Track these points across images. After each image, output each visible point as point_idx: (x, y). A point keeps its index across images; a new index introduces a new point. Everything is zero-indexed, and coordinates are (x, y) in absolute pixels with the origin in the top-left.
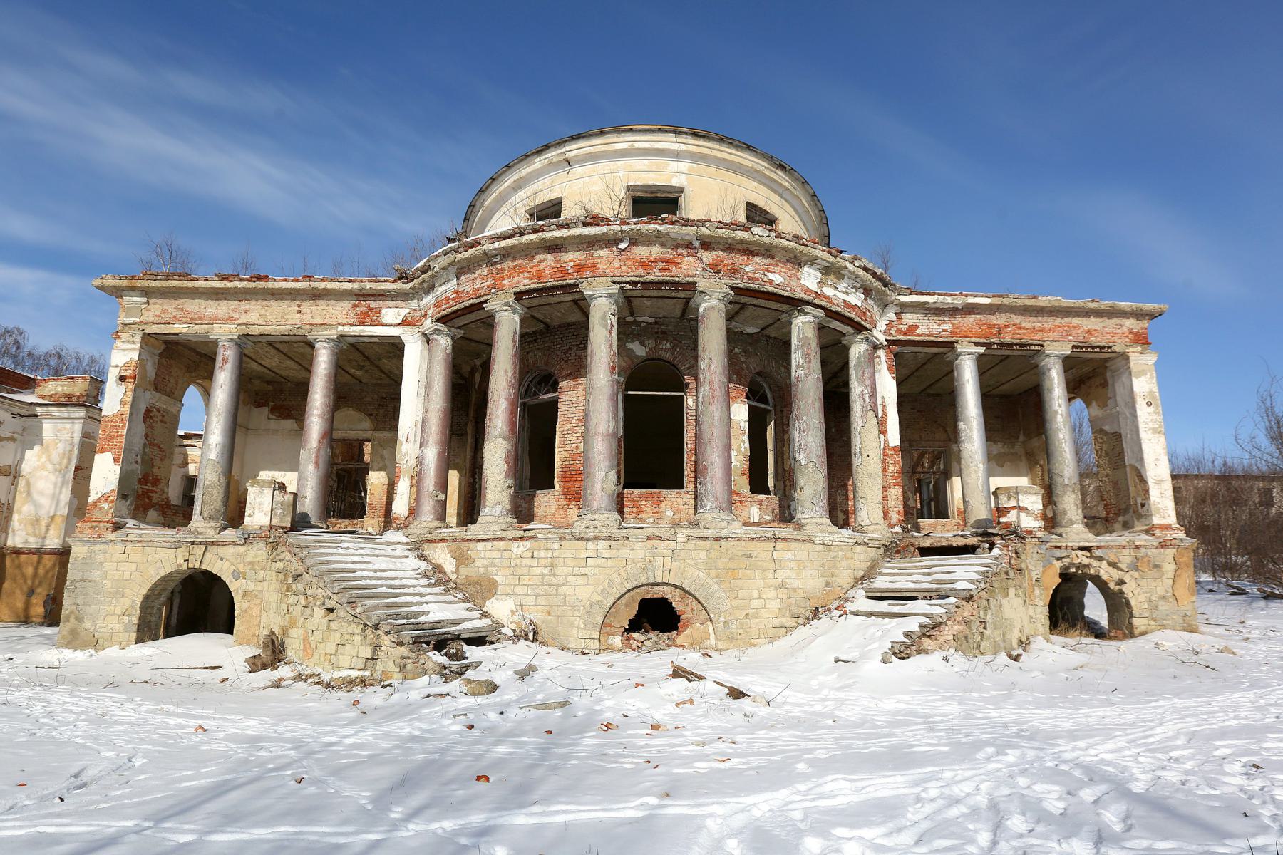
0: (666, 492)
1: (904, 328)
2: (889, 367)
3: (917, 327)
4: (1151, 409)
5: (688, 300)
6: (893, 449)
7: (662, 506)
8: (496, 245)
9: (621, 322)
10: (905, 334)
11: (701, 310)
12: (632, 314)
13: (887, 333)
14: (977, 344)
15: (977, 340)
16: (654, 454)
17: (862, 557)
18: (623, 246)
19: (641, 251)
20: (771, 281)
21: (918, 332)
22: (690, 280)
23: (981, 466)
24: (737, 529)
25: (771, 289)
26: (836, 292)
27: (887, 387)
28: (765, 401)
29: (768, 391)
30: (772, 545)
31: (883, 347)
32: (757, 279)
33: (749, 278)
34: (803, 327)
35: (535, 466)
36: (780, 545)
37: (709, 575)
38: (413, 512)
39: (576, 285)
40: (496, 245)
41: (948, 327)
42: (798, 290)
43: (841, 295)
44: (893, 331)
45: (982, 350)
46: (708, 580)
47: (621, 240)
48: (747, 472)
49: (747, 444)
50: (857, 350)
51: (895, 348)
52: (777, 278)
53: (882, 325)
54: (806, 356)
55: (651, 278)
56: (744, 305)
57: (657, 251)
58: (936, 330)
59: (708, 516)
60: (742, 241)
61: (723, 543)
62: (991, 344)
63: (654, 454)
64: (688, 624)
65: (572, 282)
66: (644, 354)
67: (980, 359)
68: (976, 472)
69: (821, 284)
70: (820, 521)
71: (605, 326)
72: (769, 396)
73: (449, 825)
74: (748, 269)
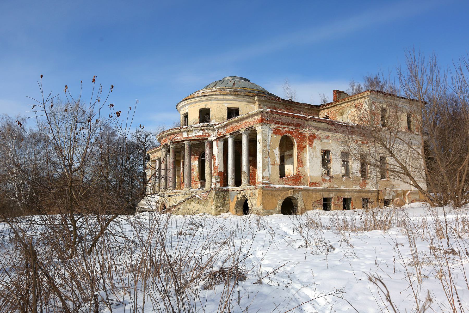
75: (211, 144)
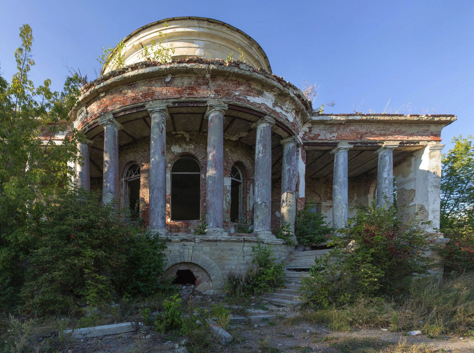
0: (191, 221)
1: (312, 136)
2: (303, 157)
3: (319, 135)
5: (204, 114)
6: (301, 199)
7: (189, 228)
8: (102, 85)
9: (168, 134)
10: (313, 139)
11: (210, 118)
12: (175, 130)
13: (303, 139)
14: (350, 143)
15: (350, 141)
17: (274, 254)
18: (168, 80)
19: (178, 82)
20: (249, 101)
21: (319, 138)
22: (204, 100)
23: (344, 206)
24: (225, 235)
25: (248, 106)
26: (281, 111)
27: (302, 167)
28: (240, 179)
29: (240, 173)
30: (242, 244)
32: (241, 100)
33: (238, 99)
34: (262, 129)
36: (246, 244)
37: (211, 258)
39: (143, 106)
40: (102, 85)
41: (335, 135)
42: (263, 107)
43: (284, 113)
44: (306, 138)
45: (352, 146)
46: (211, 261)
48: (230, 211)
49: (230, 198)
50: (289, 146)
51: (306, 147)
52: (255, 100)
53: (301, 134)
54: (264, 147)
55: (183, 99)
56: (234, 118)
57: (186, 81)
58: (329, 136)
59: (211, 230)
61: (219, 243)
62: (356, 143)
64: (200, 282)
65: (141, 104)
66: (181, 152)
67: (350, 152)
68: (342, 209)
69: (275, 105)
70: (266, 232)
71: (159, 128)
72: (241, 176)
73: (371, 138)
74: (237, 93)
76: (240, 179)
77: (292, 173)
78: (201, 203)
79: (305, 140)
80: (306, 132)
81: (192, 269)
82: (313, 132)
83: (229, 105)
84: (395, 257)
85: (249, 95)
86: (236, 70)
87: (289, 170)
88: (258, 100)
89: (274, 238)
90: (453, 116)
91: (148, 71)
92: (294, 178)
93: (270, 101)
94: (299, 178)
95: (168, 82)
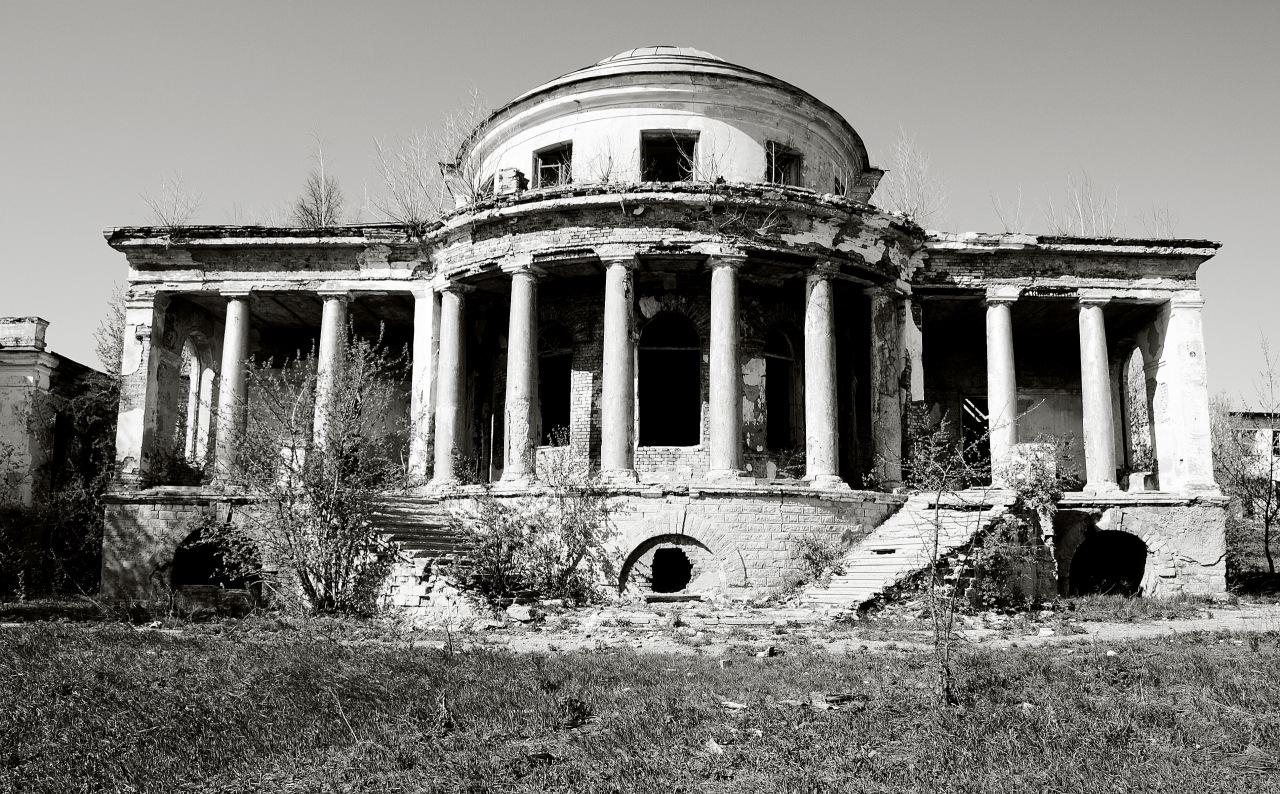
4: (1194, 360)
16: (668, 414)
18: (639, 211)
20: (784, 243)
27: (913, 338)
31: (909, 297)
35: (551, 419)
38: (430, 472)
44: (920, 279)
47: (636, 207)
49: (763, 401)
60: (754, 205)
63: (668, 414)
64: (698, 573)
69: (836, 242)
75: (897, 300)
76: (790, 356)
77: (887, 355)
78: (702, 414)
79: (918, 283)
80: (918, 269)
81: (684, 548)
82: (934, 268)
83: (748, 250)
84: (90, 509)
85: (784, 233)
86: (757, 202)
87: (882, 348)
88: (803, 239)
89: (845, 487)
90: (1217, 246)
91: (603, 202)
92: (891, 364)
93: (826, 236)
94: (908, 360)
95: (641, 216)
